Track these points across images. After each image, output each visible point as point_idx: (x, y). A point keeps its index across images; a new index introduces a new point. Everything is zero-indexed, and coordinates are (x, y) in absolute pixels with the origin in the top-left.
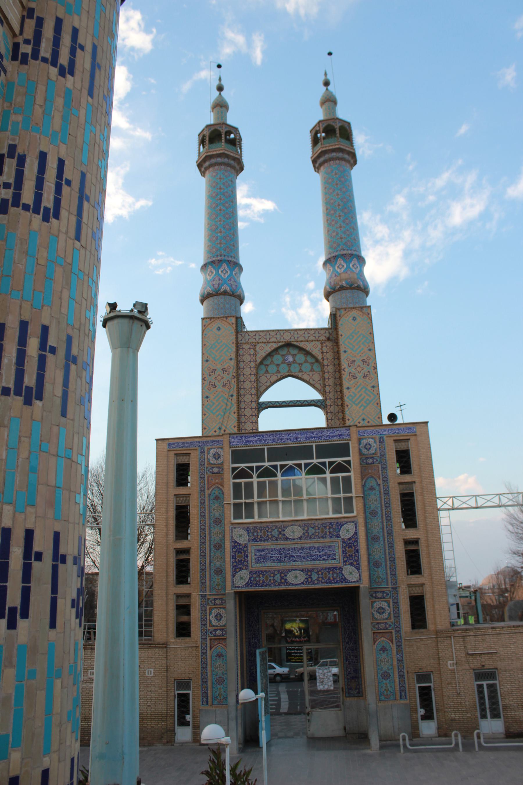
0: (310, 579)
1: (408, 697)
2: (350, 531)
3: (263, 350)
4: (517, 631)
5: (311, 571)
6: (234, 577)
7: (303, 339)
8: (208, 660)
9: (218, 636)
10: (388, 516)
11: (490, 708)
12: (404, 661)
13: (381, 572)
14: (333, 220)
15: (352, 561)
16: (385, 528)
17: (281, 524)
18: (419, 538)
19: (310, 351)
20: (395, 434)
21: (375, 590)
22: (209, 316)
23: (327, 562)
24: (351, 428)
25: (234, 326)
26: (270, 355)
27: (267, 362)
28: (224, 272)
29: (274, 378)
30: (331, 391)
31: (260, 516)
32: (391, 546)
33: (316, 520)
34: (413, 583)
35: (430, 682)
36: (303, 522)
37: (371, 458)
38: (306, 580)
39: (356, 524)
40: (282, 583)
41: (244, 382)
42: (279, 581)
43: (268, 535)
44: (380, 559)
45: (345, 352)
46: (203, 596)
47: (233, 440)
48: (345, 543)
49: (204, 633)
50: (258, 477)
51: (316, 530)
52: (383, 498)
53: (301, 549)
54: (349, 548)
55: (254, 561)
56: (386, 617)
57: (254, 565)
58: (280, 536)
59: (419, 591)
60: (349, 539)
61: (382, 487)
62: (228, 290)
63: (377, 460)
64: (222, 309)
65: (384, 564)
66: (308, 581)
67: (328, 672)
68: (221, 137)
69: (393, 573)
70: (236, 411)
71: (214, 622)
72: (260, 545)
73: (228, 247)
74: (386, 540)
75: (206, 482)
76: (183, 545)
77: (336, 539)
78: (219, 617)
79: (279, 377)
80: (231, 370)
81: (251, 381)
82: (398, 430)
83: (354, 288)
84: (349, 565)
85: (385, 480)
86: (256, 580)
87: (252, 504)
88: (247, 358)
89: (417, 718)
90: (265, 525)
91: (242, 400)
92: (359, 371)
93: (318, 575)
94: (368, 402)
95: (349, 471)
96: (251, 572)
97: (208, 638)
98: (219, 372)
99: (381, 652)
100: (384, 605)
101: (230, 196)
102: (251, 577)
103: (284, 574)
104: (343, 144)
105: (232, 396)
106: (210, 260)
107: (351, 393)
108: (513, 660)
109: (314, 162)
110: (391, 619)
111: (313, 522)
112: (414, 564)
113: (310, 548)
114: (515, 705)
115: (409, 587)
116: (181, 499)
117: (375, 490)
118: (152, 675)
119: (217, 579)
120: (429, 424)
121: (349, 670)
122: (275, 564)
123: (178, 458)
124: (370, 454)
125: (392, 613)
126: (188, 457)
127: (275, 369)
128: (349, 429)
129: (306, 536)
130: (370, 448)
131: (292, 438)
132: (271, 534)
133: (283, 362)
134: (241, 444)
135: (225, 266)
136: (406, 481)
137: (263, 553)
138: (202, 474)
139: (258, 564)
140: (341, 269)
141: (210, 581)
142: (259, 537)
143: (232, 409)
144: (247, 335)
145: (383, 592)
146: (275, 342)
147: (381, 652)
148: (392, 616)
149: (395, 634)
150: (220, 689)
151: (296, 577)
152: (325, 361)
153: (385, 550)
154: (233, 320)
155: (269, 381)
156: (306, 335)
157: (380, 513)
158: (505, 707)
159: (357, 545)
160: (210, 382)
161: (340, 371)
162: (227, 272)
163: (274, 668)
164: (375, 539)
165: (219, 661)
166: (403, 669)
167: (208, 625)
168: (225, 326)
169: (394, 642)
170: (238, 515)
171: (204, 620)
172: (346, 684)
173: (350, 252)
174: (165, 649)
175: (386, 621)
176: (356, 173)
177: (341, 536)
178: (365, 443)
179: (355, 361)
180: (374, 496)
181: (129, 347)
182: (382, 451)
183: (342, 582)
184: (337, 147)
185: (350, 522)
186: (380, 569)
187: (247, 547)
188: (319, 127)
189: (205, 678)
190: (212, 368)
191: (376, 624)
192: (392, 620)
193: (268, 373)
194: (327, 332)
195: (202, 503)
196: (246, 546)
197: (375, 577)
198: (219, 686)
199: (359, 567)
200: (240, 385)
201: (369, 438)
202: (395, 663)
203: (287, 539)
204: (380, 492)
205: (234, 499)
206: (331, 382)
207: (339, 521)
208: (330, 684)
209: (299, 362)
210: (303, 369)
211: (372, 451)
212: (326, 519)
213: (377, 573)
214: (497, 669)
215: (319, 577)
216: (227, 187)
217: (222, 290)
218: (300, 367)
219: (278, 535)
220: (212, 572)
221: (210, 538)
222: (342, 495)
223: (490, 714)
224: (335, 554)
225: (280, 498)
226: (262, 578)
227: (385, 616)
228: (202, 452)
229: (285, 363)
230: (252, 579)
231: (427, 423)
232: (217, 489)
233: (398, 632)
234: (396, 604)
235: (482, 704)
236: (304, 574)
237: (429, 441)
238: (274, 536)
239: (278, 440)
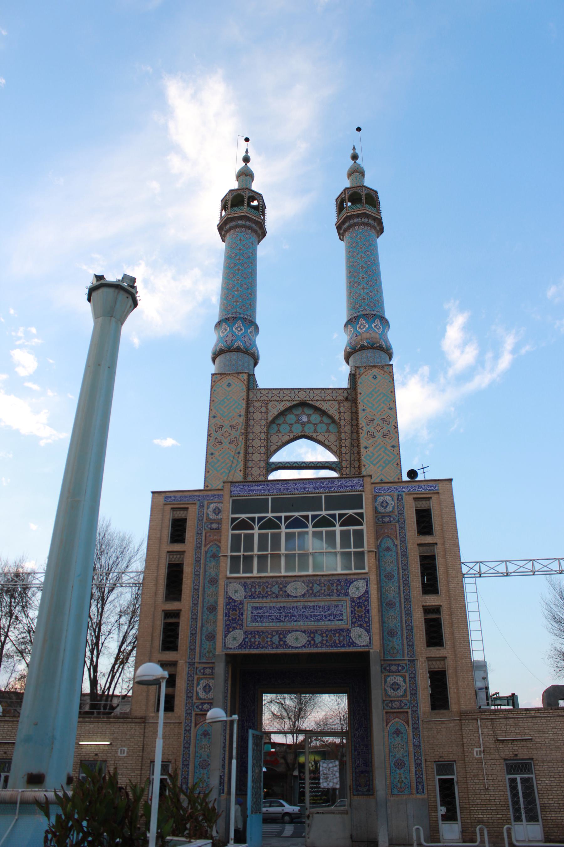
0: (312, 642)
1: (425, 791)
2: (360, 589)
3: (275, 409)
4: (556, 714)
5: (314, 632)
6: (226, 637)
7: (319, 398)
8: (192, 738)
10: (406, 580)
11: (525, 808)
12: (422, 747)
13: (396, 642)
14: (356, 282)
16: (402, 593)
17: (282, 579)
18: (441, 606)
20: (416, 492)
21: (388, 662)
22: (220, 372)
23: (333, 623)
24: (365, 478)
25: (245, 382)
26: (283, 413)
27: (280, 421)
28: (239, 329)
29: (286, 438)
30: (347, 452)
31: (259, 571)
32: (409, 614)
33: (323, 576)
34: (433, 656)
35: (453, 774)
36: (308, 578)
37: (388, 516)
38: (308, 643)
39: (367, 582)
40: (280, 645)
41: (253, 440)
42: (277, 643)
43: (267, 592)
44: (396, 627)
45: (364, 410)
46: (191, 664)
47: (234, 489)
48: (354, 602)
50: (259, 529)
51: (321, 587)
52: (400, 559)
53: (304, 607)
54: (358, 607)
55: (249, 620)
56: (401, 694)
57: (249, 624)
58: (281, 592)
59: (440, 666)
60: (359, 598)
61: (399, 548)
62: (242, 347)
63: (394, 519)
64: (233, 365)
65: (399, 633)
66: (310, 644)
67: (333, 767)
68: (244, 203)
69: (410, 643)
70: (242, 469)
71: (202, 695)
72: (258, 602)
73: (243, 305)
74: (403, 606)
75: (203, 538)
76: (173, 606)
78: (207, 689)
79: (292, 436)
80: (239, 427)
81: (260, 440)
82: (419, 487)
83: (376, 348)
84: (358, 626)
85: (403, 541)
86: (250, 641)
87: (251, 557)
88: (257, 416)
89: (437, 818)
90: (264, 580)
91: (250, 459)
92: (379, 430)
93: (323, 637)
94: (387, 462)
95: (362, 525)
96: (246, 632)
97: (194, 713)
98: (226, 428)
99: (395, 735)
100: (399, 680)
101: (249, 258)
102: (246, 638)
103: (283, 635)
104: (369, 210)
105: (239, 453)
106: (224, 317)
107: (368, 453)
108: (551, 749)
109: (339, 228)
110: (407, 697)
111: (318, 578)
112: (435, 636)
113: (314, 606)
114: (556, 805)
115: (429, 661)
116: (175, 556)
117: (391, 551)
118: (125, 754)
119: (207, 645)
120: (453, 482)
122: (274, 623)
123: (175, 512)
124: (387, 513)
125: (408, 689)
126: (185, 512)
127: (288, 428)
128: (363, 480)
129: (310, 593)
130: (387, 506)
131: (299, 487)
132: (271, 591)
133: (297, 422)
134: (242, 493)
135: (239, 323)
136: (426, 542)
137: (260, 611)
138: (200, 530)
139: (254, 624)
140: (362, 329)
141: (201, 647)
142: (257, 593)
143: (238, 467)
144: (259, 392)
145: (399, 665)
146: (289, 401)
147: (395, 735)
148: (408, 693)
149: (412, 714)
150: (203, 774)
151: (297, 639)
152: (342, 421)
153: (401, 618)
154: (245, 376)
155: (280, 441)
156: (323, 395)
157: (396, 576)
158: (544, 808)
159: (368, 604)
160: (216, 438)
161: (358, 432)
162: (241, 329)
163: (284, 806)
164: (391, 605)
165: (205, 741)
166: (421, 756)
167: (194, 697)
168: (236, 383)
170: (235, 568)
171: (190, 692)
172: (354, 779)
173: (372, 312)
174: (143, 724)
175: (401, 699)
176: (381, 241)
177: (350, 594)
178: (381, 501)
179: (374, 420)
180: (390, 559)
181: (112, 316)
182: (401, 509)
183: (349, 646)
184: (362, 212)
185: (361, 579)
186: (395, 639)
187: (243, 604)
188: (345, 194)
189: (186, 760)
190: (220, 424)
191: (387, 702)
192: (409, 697)
193: (280, 432)
194: (345, 392)
195: (198, 561)
196: (241, 603)
197: (389, 647)
198: (202, 771)
199: (369, 629)
200: (248, 443)
201: (386, 495)
202: (411, 748)
203: (289, 596)
204: (397, 553)
205: (232, 551)
206: (347, 443)
207: (349, 577)
208: (335, 781)
210: (319, 429)
211: (389, 509)
212: (333, 575)
213: (391, 643)
214: (532, 759)
215: (323, 640)
216: (247, 249)
217: (235, 346)
218: (315, 428)
219: (279, 592)
220: (204, 637)
221: (204, 599)
222: (352, 550)
223: (526, 817)
224: (342, 614)
225: (283, 551)
226: (257, 640)
227: (400, 692)
228: (201, 506)
229: (298, 423)
230: (247, 640)
231: (451, 480)
232: (215, 546)
233: (415, 712)
234: (413, 679)
235: (516, 802)
236: (306, 636)
237: (453, 499)
238: (274, 593)
239: (284, 489)
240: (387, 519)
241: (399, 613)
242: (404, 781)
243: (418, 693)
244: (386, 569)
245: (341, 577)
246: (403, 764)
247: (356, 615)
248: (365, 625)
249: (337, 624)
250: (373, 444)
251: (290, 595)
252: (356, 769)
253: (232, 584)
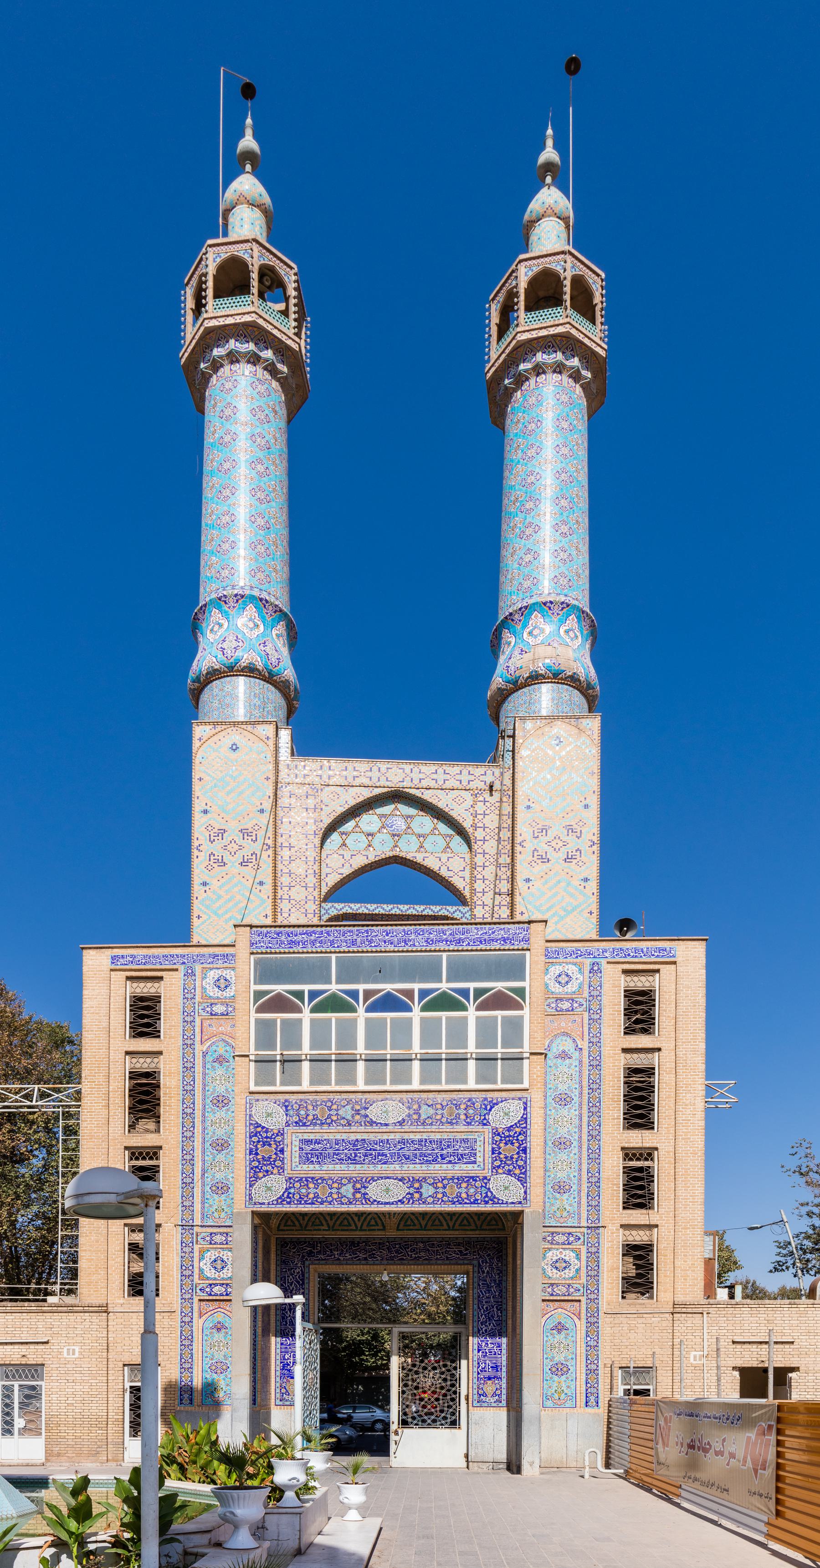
0: (417, 1196)
9: (216, 1295)
15: (511, 1167)
17: (360, 1096)
19: (447, 810)
23: (457, 1167)
27: (349, 826)
37: (568, 1000)
40: (355, 1199)
42: (350, 1196)
48: (499, 1134)
54: (506, 1144)
56: (571, 1275)
58: (357, 1117)
60: (509, 1129)
61: (585, 1053)
71: (210, 1273)
75: (198, 1030)
78: (219, 1264)
84: (504, 1173)
94: (570, 909)
97: (196, 1299)
100: (569, 1255)
113: (421, 1141)
118: (77, 1355)
121: (483, 1365)
137: (317, 1146)
140: (536, 637)
141: (203, 1203)
142: (310, 1118)
151: (387, 1190)
167: (196, 1276)
169: (583, 1316)
173: (563, 599)
183: (487, 1203)
187: (282, 1134)
190: (217, 826)
196: (281, 1133)
203: (372, 1123)
204: (581, 1062)
209: (418, 830)
211: (571, 988)
219: (353, 1116)
220: (207, 1188)
221: (204, 1129)
224: (475, 1154)
230: (292, 1191)
232: (221, 1044)
234: (594, 1256)
240: (566, 1005)
241: (576, 1156)
242: (566, 1391)
243: (600, 1275)
244: (557, 1088)
245: (474, 1095)
246: (565, 1369)
247: (502, 1156)
248: (517, 1172)
249: (463, 1169)
250: (543, 874)
251: (375, 1122)
252: (478, 1373)
253: (261, 1102)
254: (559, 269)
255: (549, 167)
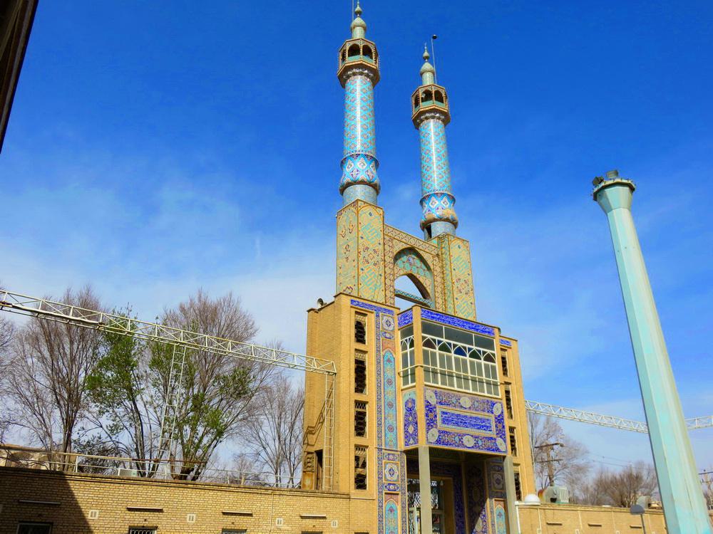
49: (381, 486)
77: (491, 415)
118: (194, 522)
203: (462, 407)
254: (430, 90)
255: (427, 57)
